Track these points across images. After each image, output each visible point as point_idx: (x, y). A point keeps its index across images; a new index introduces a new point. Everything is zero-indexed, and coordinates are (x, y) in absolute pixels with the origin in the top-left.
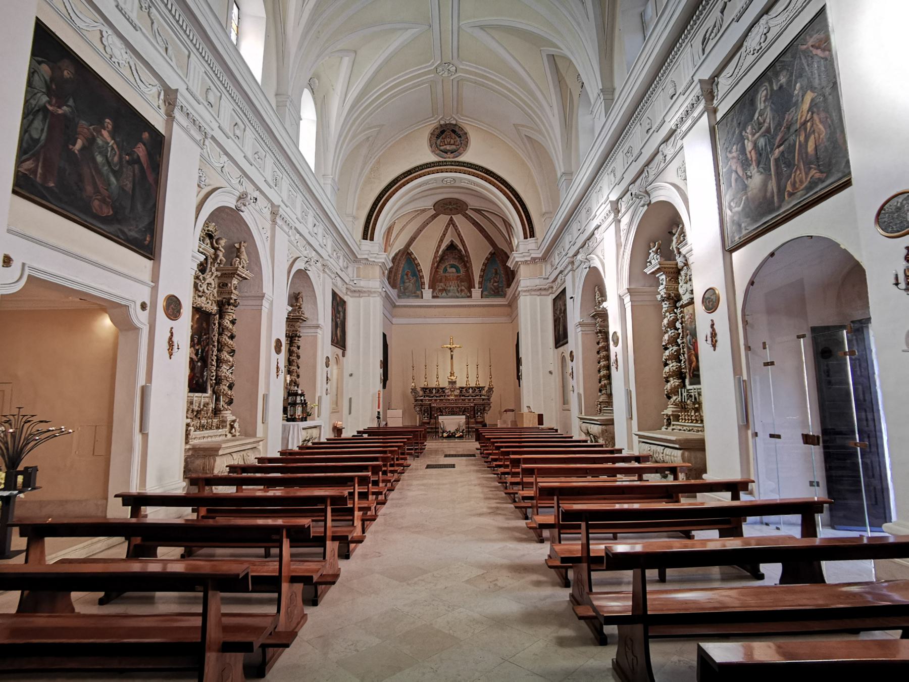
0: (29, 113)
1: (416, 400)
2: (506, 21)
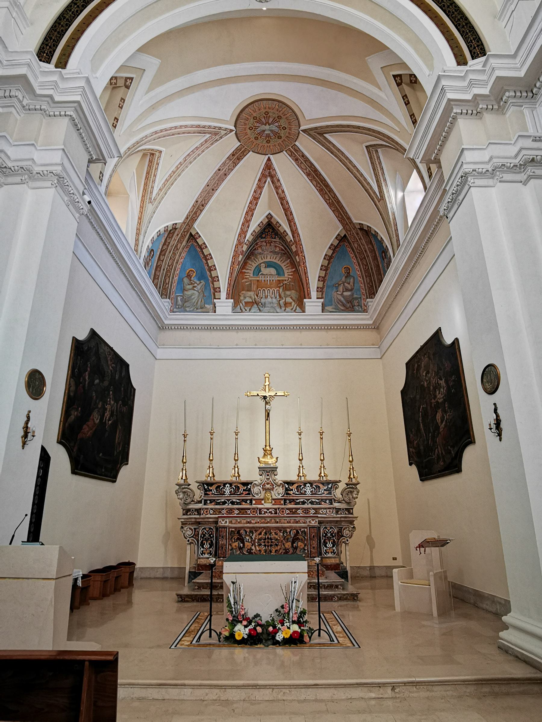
1: (187, 511)
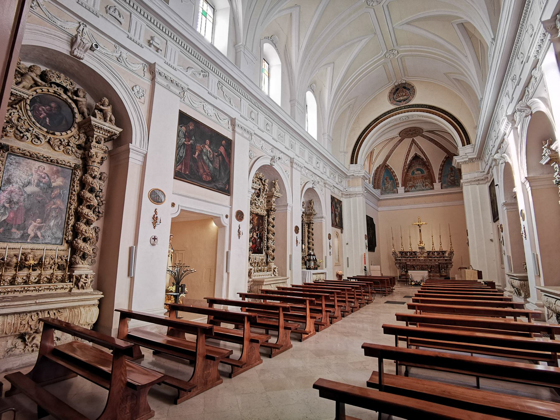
0: (178, 147)
1: (396, 260)
2: (422, 14)
